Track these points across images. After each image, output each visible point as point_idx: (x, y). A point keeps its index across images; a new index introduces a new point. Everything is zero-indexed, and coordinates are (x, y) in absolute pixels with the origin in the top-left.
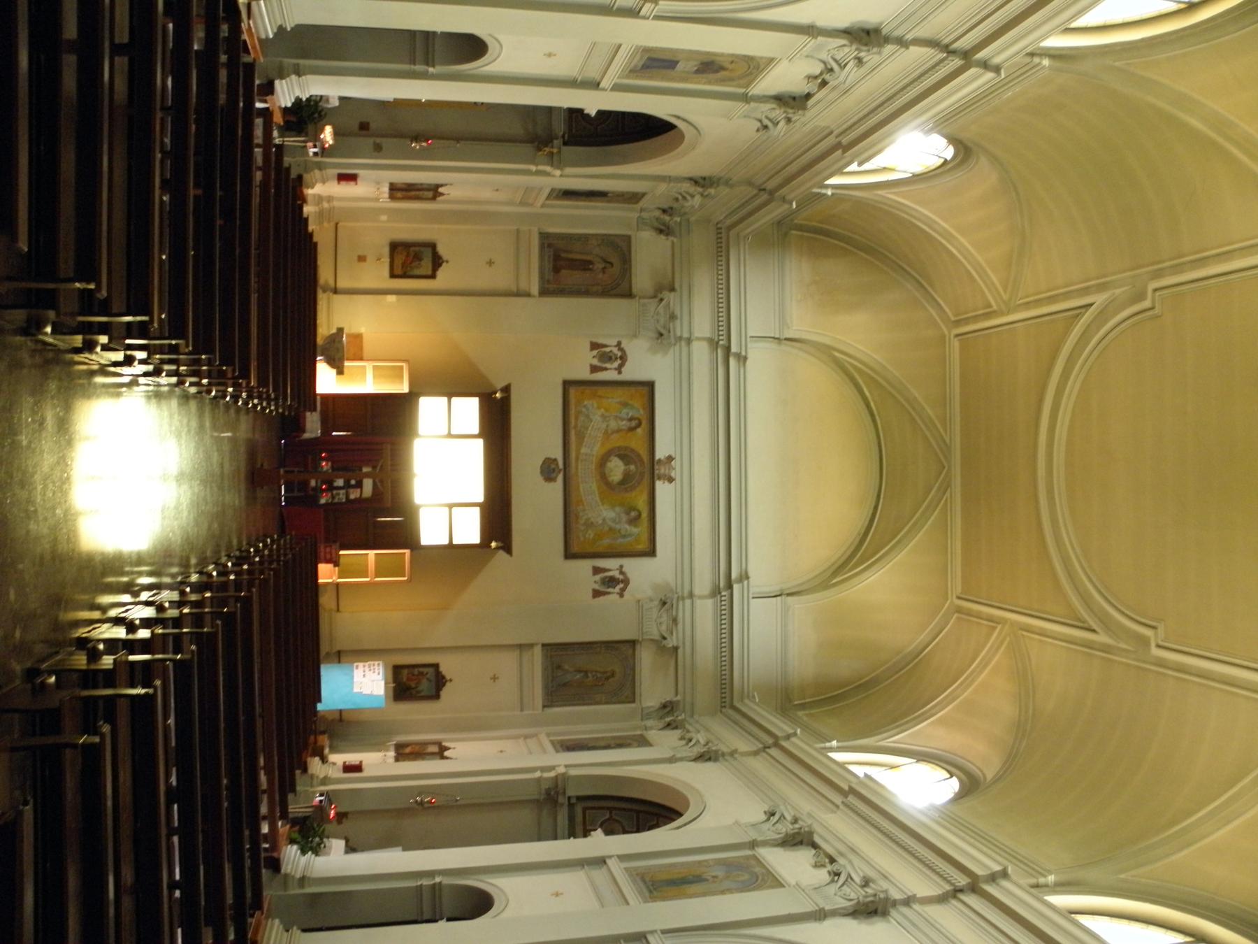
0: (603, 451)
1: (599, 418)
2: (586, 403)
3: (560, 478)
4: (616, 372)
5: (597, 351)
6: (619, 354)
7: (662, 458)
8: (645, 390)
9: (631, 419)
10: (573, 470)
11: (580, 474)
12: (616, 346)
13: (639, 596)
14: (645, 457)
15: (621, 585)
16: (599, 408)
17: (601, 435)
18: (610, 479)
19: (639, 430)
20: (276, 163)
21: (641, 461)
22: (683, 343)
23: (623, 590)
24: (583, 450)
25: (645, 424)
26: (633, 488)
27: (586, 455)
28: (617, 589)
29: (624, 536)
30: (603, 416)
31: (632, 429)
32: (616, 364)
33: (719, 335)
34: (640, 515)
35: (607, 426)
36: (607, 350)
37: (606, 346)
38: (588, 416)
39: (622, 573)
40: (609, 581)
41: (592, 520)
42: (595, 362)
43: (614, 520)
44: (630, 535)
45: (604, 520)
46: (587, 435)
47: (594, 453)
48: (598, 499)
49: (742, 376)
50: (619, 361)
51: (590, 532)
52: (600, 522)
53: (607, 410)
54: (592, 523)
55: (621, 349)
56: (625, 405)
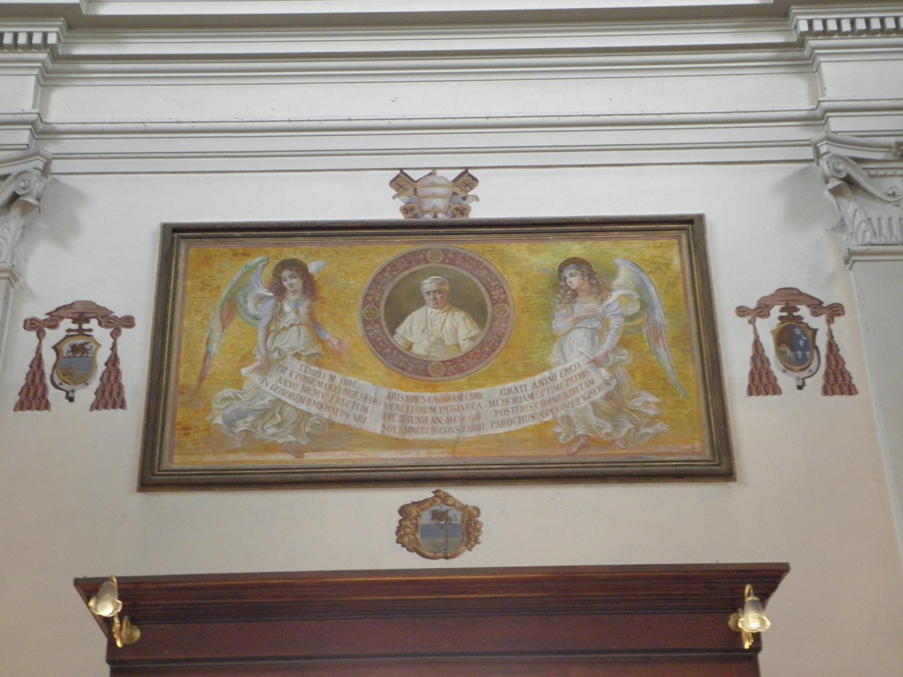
0: (377, 368)
1: (272, 380)
2: (219, 420)
3: (463, 495)
4: (125, 331)
5: (51, 390)
6: (67, 324)
7: (400, 203)
8: (186, 250)
9: (279, 291)
10: (438, 456)
11: (452, 436)
12: (41, 335)
13: (832, 261)
14: (399, 248)
15: (804, 311)
16: (238, 382)
17: (326, 373)
18: (466, 346)
19: (313, 267)
20: (167, 366)
21: (408, 259)
22: (51, 148)
23: (816, 306)
24: (374, 425)
25: (292, 251)
26: (495, 284)
27: (387, 417)
28: (818, 323)
29: (645, 305)
30: (265, 368)
31: (310, 286)
32: (101, 334)
33: (30, 46)
34: (577, 262)
35: (298, 355)
36: (49, 359)
37: (38, 361)
38: (264, 413)
39: (762, 310)
40: (793, 347)
41: (598, 397)
42: (86, 394)
43: (598, 334)
44: (641, 288)
45: (596, 363)
46: (326, 415)
47: (383, 392)
48: (528, 381)
49: (149, 155)
50: (94, 323)
51: (637, 403)
52: (604, 372)
53: (247, 359)
54: (608, 397)
55: (53, 320)
56: (231, 308)
